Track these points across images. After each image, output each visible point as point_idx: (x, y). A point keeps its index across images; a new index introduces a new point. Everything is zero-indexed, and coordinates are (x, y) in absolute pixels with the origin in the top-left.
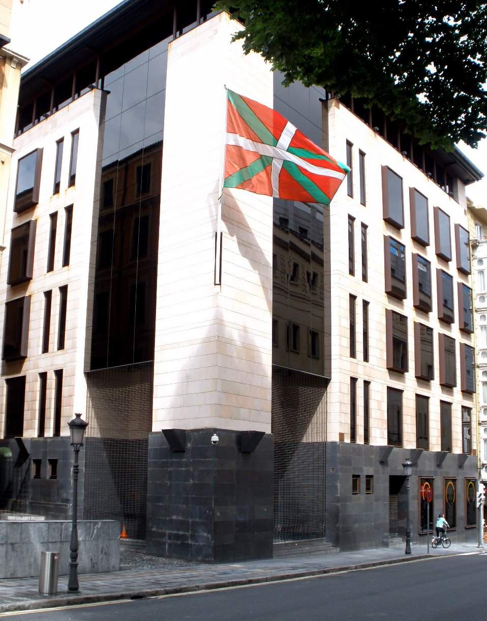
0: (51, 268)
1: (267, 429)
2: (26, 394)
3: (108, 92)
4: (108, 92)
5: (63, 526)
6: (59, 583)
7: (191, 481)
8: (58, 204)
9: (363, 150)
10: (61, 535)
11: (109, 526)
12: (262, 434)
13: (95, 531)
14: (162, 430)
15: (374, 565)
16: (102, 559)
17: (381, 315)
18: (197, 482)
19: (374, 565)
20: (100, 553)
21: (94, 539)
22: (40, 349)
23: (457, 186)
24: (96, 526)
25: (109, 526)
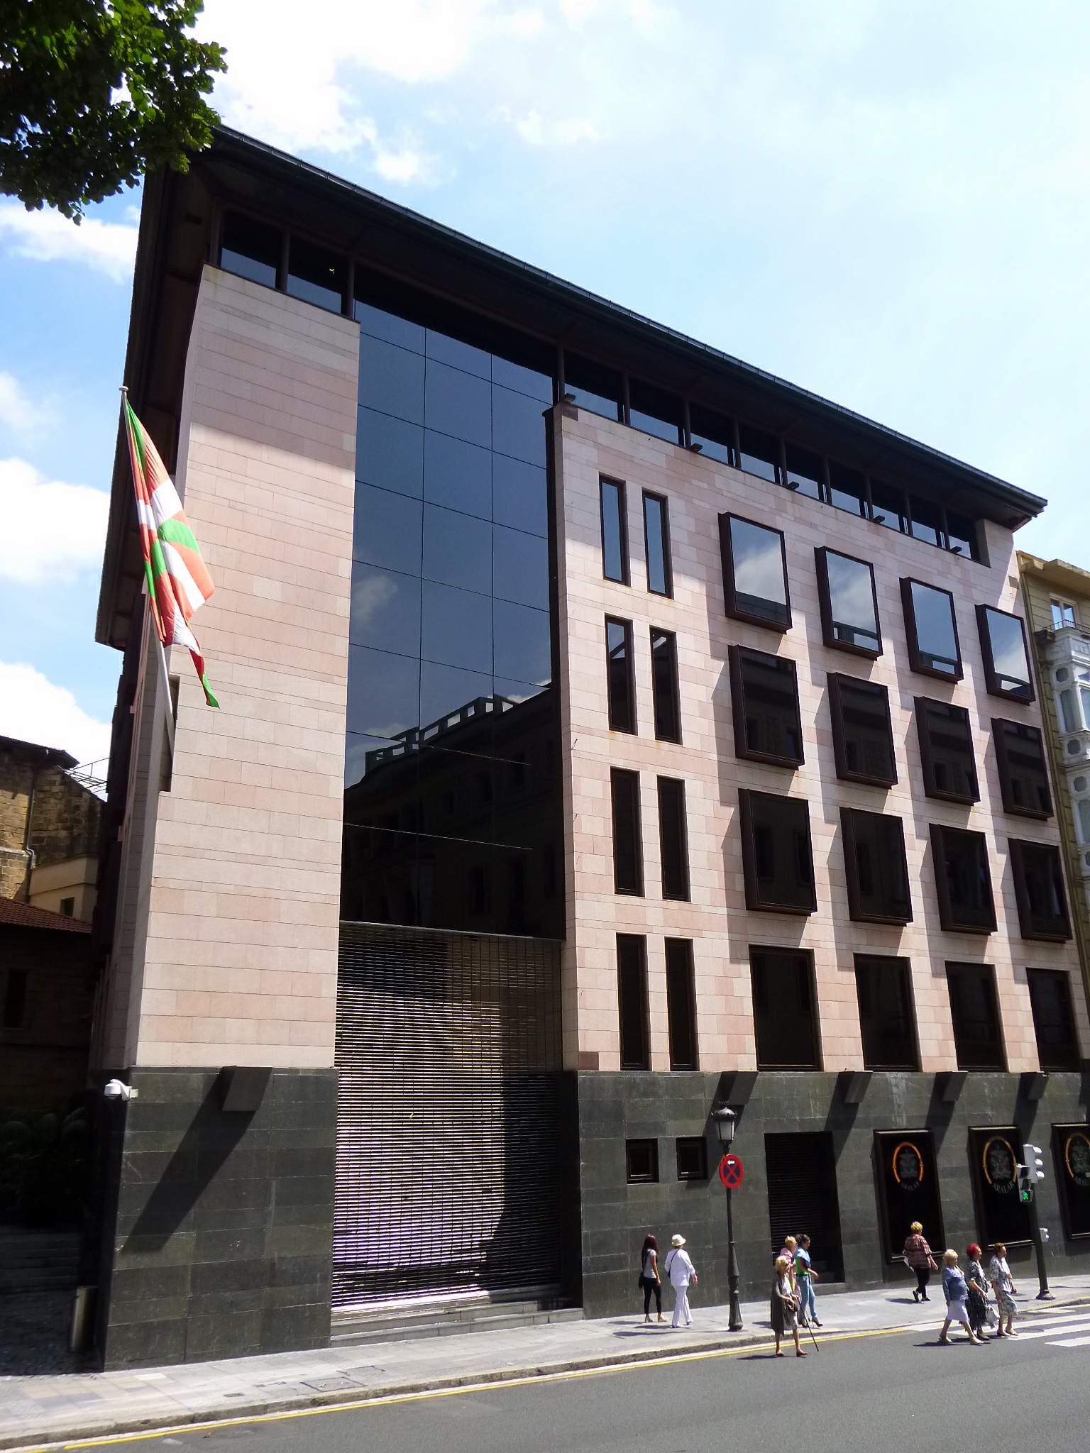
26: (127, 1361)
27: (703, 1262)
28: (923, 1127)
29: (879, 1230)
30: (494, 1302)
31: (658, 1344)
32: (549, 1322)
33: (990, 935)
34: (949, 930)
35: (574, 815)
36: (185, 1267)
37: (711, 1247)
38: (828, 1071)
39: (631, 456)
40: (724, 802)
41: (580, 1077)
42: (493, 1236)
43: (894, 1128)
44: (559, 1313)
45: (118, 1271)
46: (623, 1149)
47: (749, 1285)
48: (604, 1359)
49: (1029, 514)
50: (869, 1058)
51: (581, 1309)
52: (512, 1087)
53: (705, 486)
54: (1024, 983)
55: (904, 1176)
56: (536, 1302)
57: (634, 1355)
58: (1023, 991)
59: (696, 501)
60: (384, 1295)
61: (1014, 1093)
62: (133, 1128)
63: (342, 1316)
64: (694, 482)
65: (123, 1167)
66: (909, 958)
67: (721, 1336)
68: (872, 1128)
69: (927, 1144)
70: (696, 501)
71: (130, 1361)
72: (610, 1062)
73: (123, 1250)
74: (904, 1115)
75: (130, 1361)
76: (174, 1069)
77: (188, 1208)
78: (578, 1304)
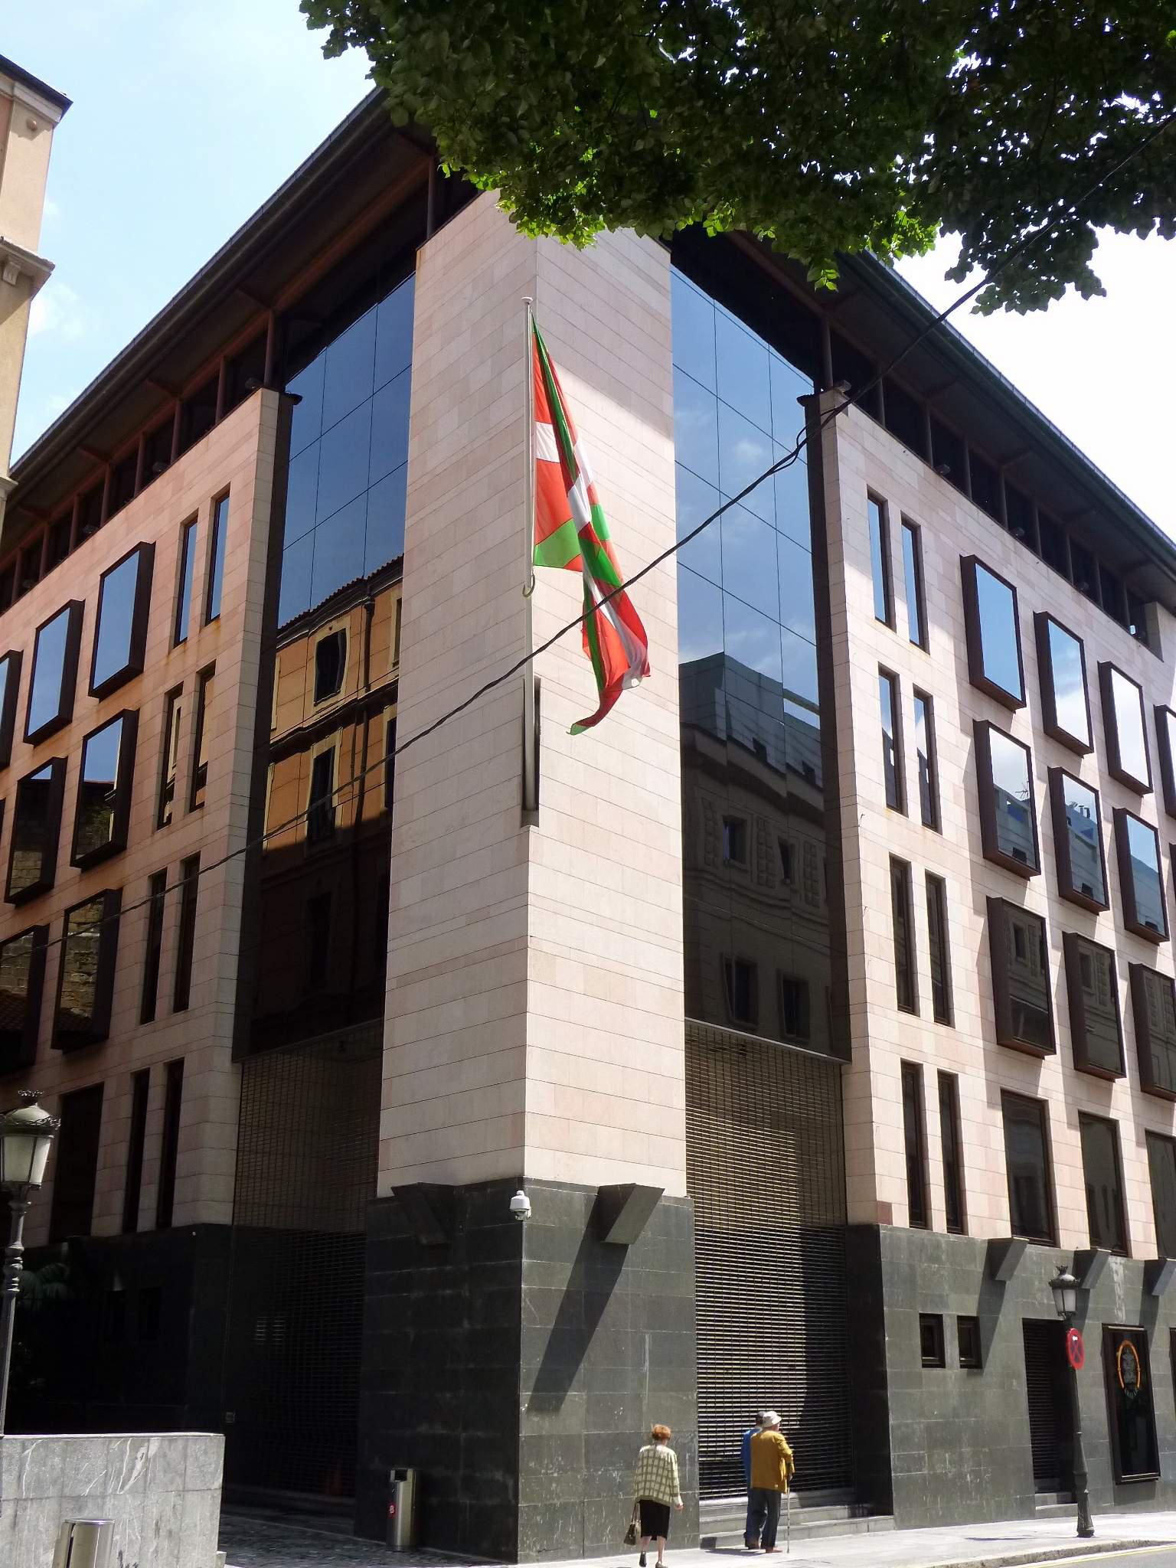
0: (148, 1013)
1: (674, 1184)
2: (103, 1128)
3: (297, 399)
4: (297, 399)
5: (28, 1452)
6: (739, 1507)
7: (466, 1325)
8: (184, 667)
9: (925, 687)
10: (20, 1477)
11: (185, 1448)
12: (654, 1194)
13: (139, 1465)
14: (394, 1189)
15: (562, 403)
16: (156, 1551)
17: (976, 1016)
18: (479, 1327)
19: (562, 403)
20: (151, 1533)
21: (133, 1491)
22: (135, 1013)
23: (1157, 618)
24: (143, 1450)
25: (185, 1448)
26: (536, 1551)
27: (982, 1468)
28: (1137, 1324)
29: (1109, 1442)
30: (803, 1506)
31: (992, 1552)
32: (868, 1531)
33: (1114, 1082)
34: (1149, 1093)
35: (863, 908)
36: (580, 1436)
37: (987, 1450)
38: (1137, 1259)
39: (891, 470)
40: (977, 912)
41: (881, 1231)
42: (799, 1425)
43: (1116, 1323)
44: (876, 1520)
45: (525, 1437)
46: (918, 1324)
47: (1017, 1499)
48: (1025, 1556)
49: (857, 257)
50: (1016, 1228)
51: (892, 1517)
52: (810, 1236)
53: (949, 519)
54: (1075, 1129)
55: (1126, 1381)
56: (846, 1507)
57: (1044, 1553)
58: (1075, 1138)
59: (942, 536)
60: (710, 1491)
61: (978, 1267)
62: (530, 1257)
63: (711, 1512)
64: (942, 513)
65: (523, 1304)
66: (1047, 1101)
67: (1071, 1542)
68: (1101, 1322)
69: (1141, 1340)
70: (942, 536)
71: (539, 1551)
72: (901, 1217)
73: (528, 1409)
74: (1123, 1308)
75: (539, 1551)
76: (560, 1185)
77: (578, 1363)
78: (888, 1511)
